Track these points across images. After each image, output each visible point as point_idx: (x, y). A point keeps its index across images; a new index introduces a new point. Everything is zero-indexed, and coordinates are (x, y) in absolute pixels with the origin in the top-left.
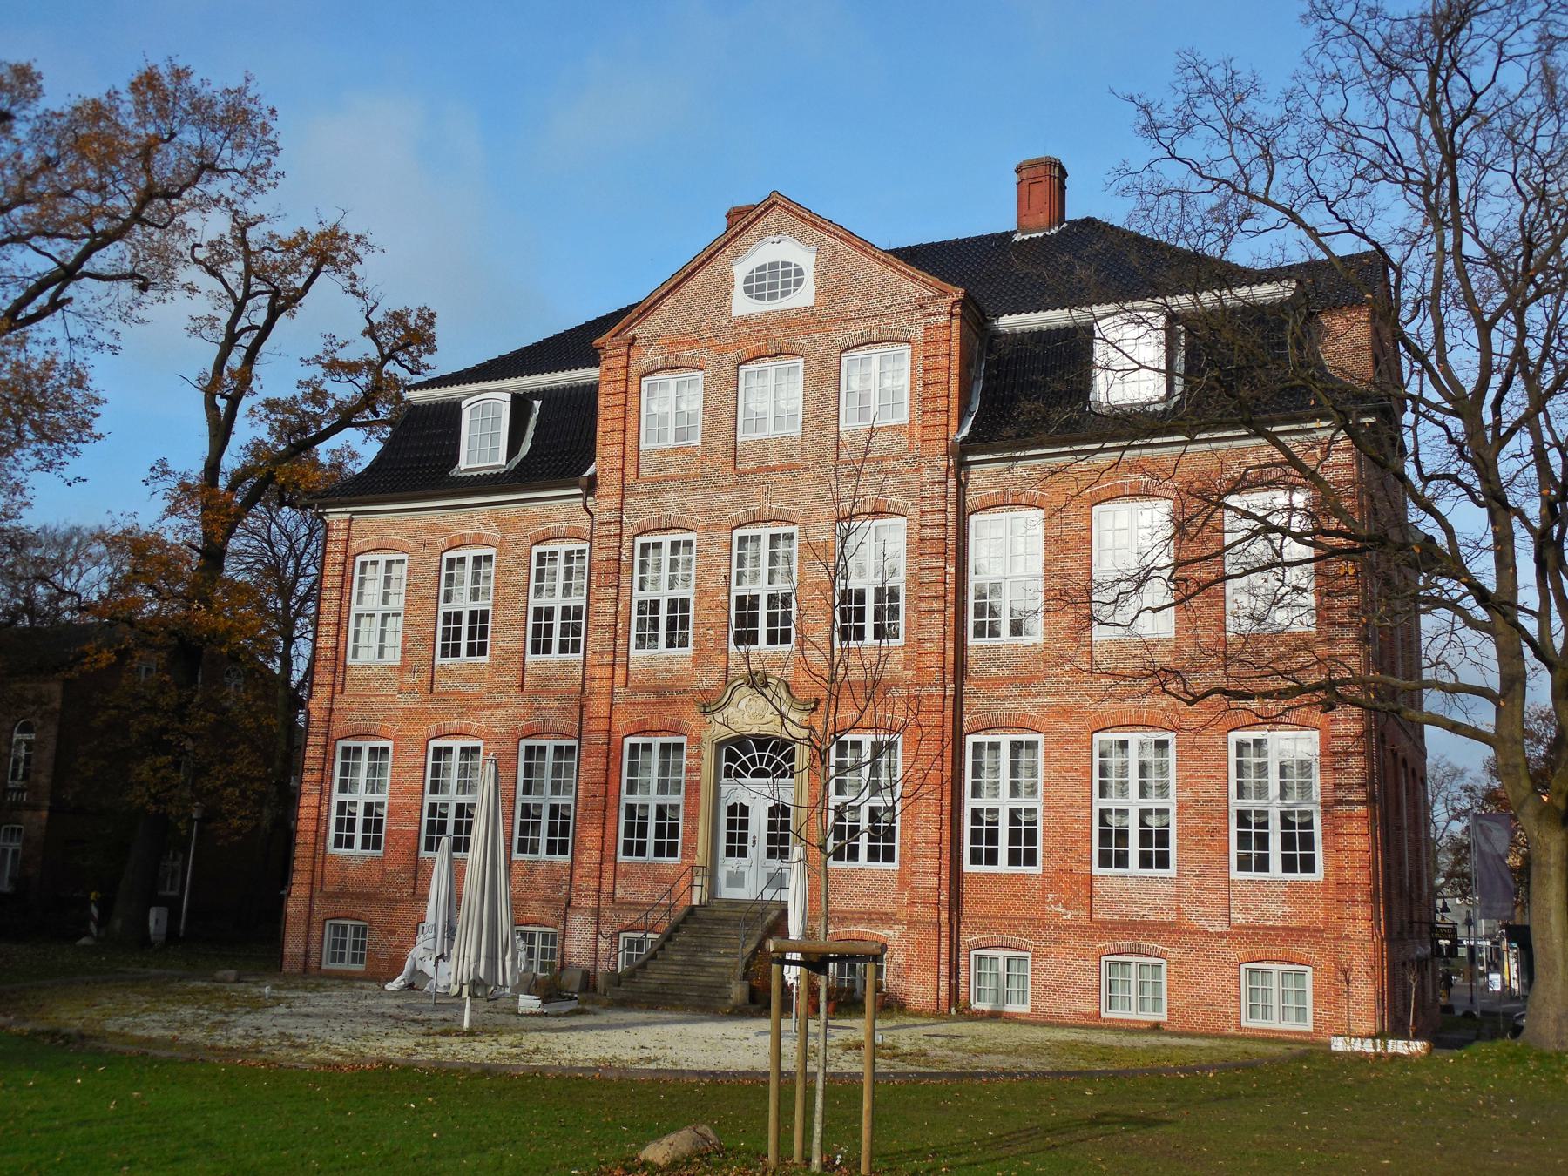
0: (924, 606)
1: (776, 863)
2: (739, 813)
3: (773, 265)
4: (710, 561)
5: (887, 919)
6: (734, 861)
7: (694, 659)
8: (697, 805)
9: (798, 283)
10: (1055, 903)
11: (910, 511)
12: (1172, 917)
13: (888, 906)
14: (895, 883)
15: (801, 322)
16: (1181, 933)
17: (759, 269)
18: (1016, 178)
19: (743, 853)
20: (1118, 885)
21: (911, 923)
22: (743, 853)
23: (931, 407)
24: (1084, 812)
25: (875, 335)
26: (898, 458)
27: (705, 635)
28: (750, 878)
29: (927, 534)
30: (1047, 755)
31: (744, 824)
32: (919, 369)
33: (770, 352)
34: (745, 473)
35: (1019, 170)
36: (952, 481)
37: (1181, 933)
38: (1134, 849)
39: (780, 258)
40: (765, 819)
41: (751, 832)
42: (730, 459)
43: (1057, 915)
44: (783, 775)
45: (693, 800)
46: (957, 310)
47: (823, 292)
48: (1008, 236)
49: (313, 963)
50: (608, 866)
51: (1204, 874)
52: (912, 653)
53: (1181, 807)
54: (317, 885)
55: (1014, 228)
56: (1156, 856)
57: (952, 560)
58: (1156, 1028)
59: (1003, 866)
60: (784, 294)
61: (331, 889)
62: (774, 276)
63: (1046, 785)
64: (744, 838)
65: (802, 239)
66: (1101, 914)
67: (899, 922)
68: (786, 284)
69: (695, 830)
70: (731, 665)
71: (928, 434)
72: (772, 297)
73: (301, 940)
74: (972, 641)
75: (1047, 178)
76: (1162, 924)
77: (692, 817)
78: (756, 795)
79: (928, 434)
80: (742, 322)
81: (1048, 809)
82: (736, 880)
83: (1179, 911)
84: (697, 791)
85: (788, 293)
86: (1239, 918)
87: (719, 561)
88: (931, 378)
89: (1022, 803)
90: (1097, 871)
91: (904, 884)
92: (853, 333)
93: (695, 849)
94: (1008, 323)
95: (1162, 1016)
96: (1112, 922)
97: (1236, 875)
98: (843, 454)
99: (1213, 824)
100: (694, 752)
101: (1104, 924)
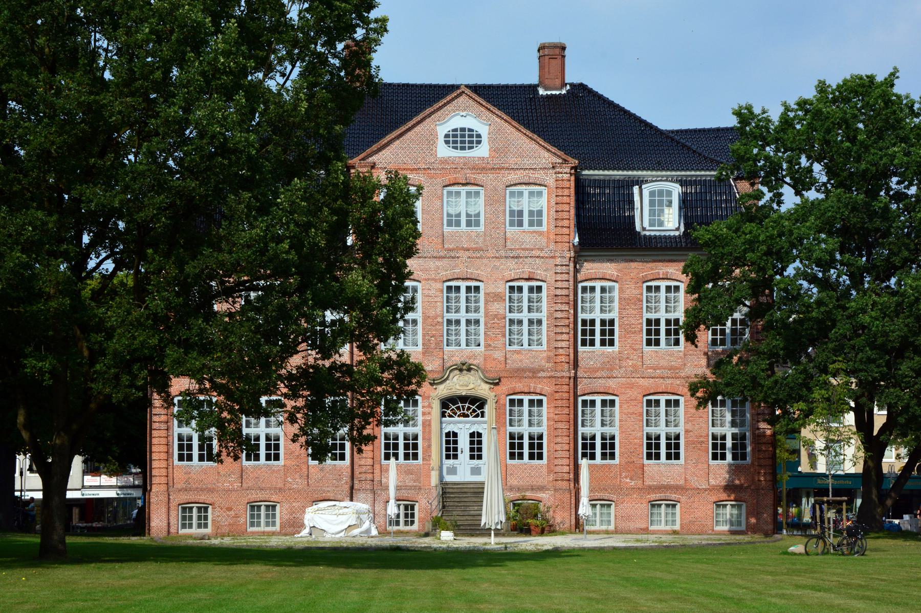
0: (558, 330)
1: (476, 462)
2: (452, 437)
3: (463, 130)
4: (430, 299)
5: (542, 489)
6: (451, 461)
7: (424, 353)
8: (430, 432)
9: (479, 142)
10: (626, 477)
11: (548, 279)
12: (682, 482)
13: (540, 482)
14: (545, 470)
15: (481, 167)
16: (687, 490)
17: (453, 130)
18: (537, 55)
19: (455, 457)
20: (656, 468)
21: (555, 490)
22: (455, 457)
23: (560, 224)
24: (639, 434)
25: (526, 180)
26: (542, 250)
27: (429, 340)
28: (460, 470)
29: (559, 292)
30: (621, 407)
31: (456, 442)
32: (553, 202)
33: (464, 182)
34: (449, 250)
35: (541, 48)
36: (572, 265)
37: (687, 490)
38: (663, 451)
39: (467, 126)
40: (468, 439)
41: (460, 446)
42: (440, 241)
43: (627, 483)
44: (477, 416)
45: (427, 430)
46: (573, 171)
47: (494, 150)
48: (533, 88)
49: (173, 530)
50: (377, 467)
51: (697, 462)
52: (552, 354)
53: (687, 431)
54: (171, 484)
55: (537, 82)
56: (673, 454)
57: (572, 307)
58: (675, 532)
59: (598, 460)
60: (470, 148)
61: (179, 487)
62: (463, 136)
63: (621, 421)
64: (456, 449)
65: (478, 116)
66: (648, 482)
67: (548, 489)
68: (471, 142)
69: (429, 446)
70: (445, 357)
71: (559, 238)
72: (463, 148)
73: (164, 516)
74: (581, 349)
75: (552, 55)
76: (677, 486)
77: (428, 439)
78: (463, 427)
79: (559, 238)
80: (445, 161)
81: (621, 432)
82: (453, 471)
83: (686, 480)
84: (430, 425)
85: (472, 148)
86: (712, 482)
87: (436, 299)
88: (560, 208)
89: (608, 430)
90: (646, 462)
91: (550, 471)
92: (513, 177)
93: (430, 456)
94: (586, 172)
95: (677, 527)
96: (653, 485)
97: (712, 462)
98: (508, 243)
99: (702, 439)
100: (426, 404)
101: (650, 487)
